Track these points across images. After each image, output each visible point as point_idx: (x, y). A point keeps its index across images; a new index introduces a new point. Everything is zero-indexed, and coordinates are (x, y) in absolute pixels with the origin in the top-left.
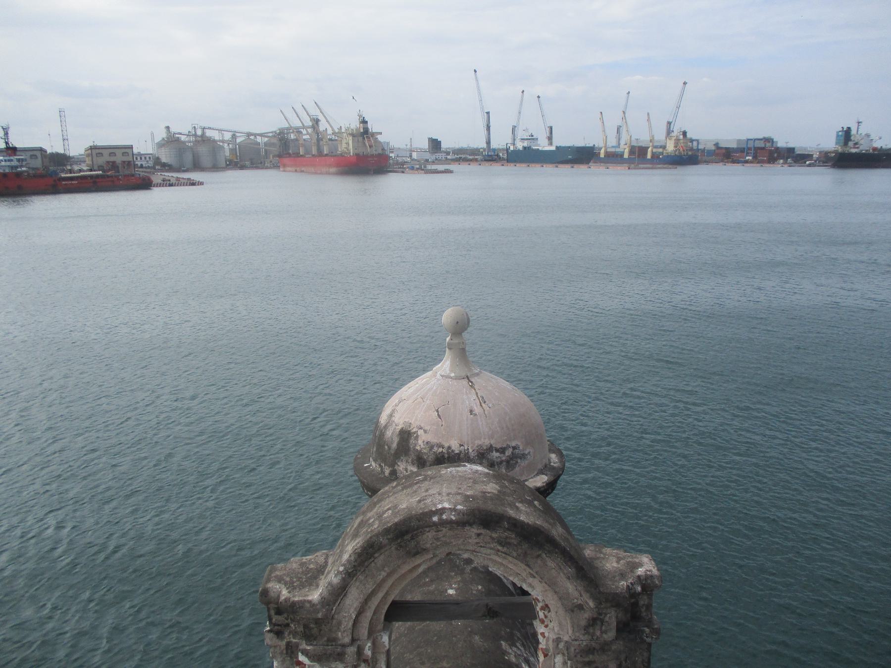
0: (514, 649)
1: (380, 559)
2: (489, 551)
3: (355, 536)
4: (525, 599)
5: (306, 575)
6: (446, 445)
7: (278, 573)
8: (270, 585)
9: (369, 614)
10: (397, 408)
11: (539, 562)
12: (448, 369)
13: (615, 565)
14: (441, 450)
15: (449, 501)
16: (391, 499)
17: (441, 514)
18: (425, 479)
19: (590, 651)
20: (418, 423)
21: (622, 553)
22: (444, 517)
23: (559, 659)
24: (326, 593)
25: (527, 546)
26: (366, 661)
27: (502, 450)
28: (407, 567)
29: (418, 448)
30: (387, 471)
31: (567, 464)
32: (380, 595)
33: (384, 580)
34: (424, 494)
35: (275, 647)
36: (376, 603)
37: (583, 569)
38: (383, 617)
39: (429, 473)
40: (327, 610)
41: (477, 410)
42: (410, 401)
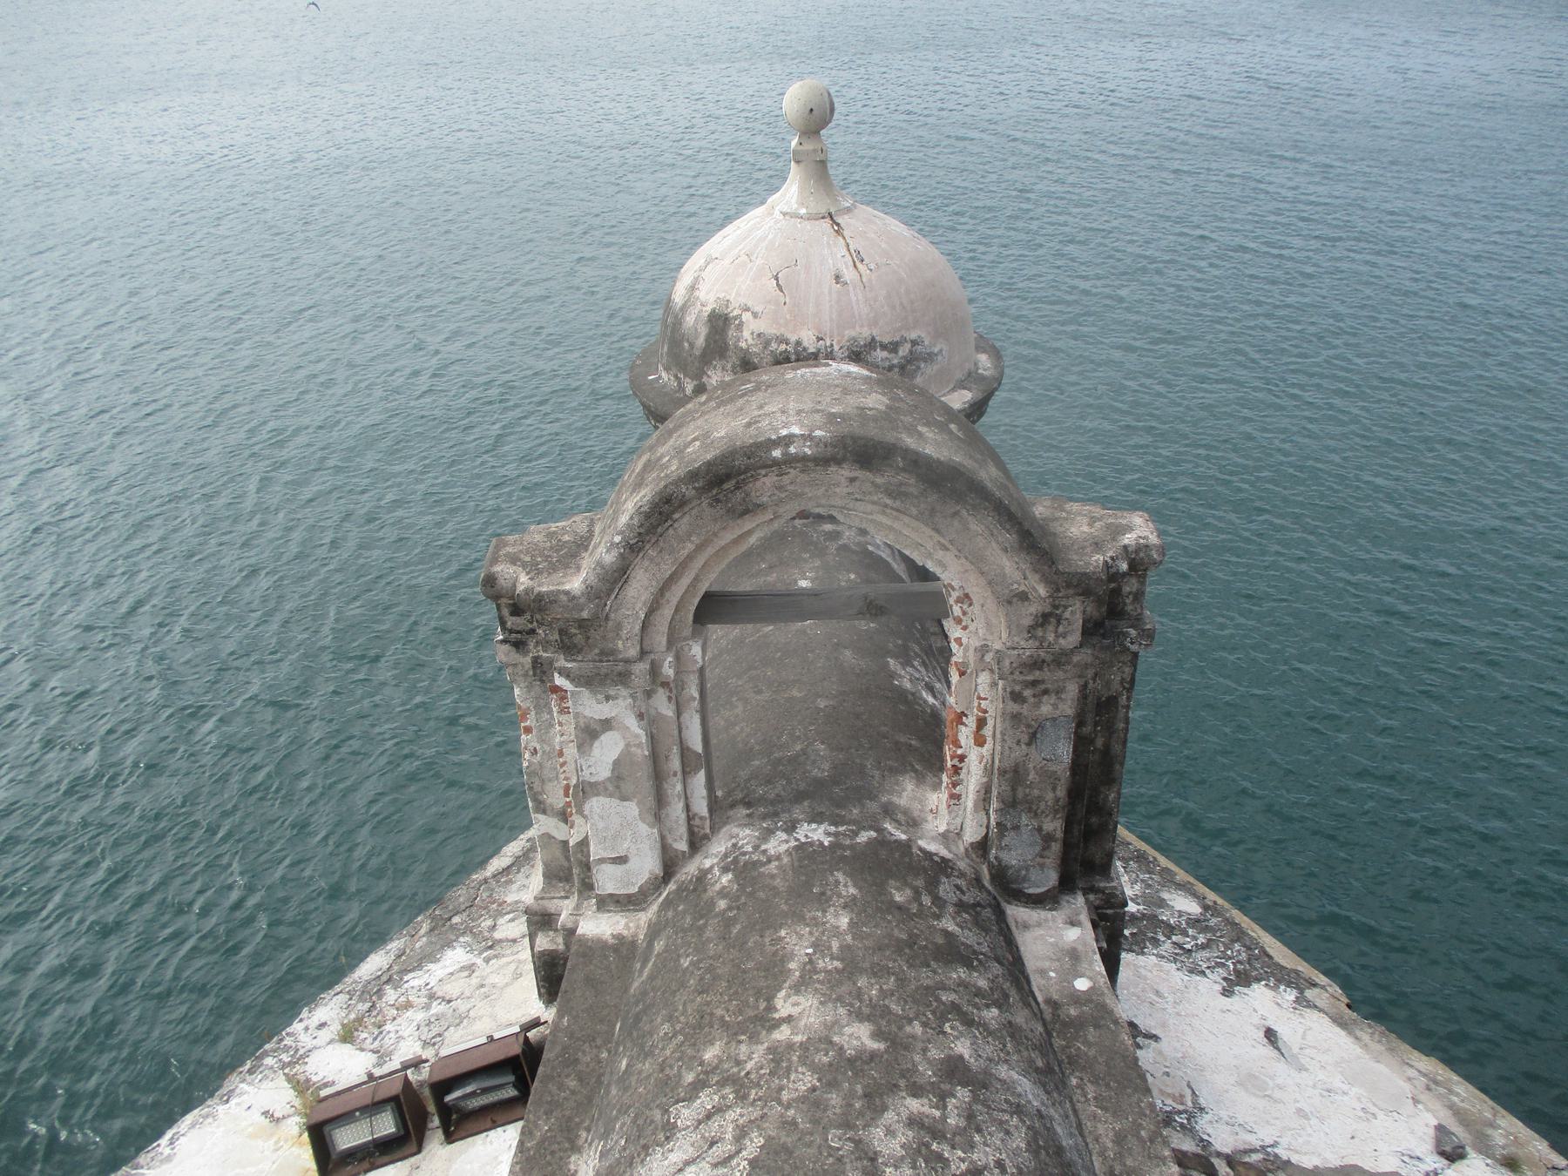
0: (909, 669)
1: (683, 523)
2: (869, 507)
3: (638, 485)
4: (929, 586)
5: (557, 551)
6: (793, 338)
7: (509, 549)
8: (497, 568)
9: (667, 612)
10: (703, 274)
11: (956, 523)
12: (794, 200)
13: (1085, 529)
14: (783, 347)
15: (800, 423)
16: (699, 422)
17: (787, 445)
18: (757, 389)
19: (1036, 664)
20: (742, 300)
21: (1098, 511)
22: (792, 450)
23: (984, 679)
24: (593, 580)
25: (935, 497)
26: (665, 685)
27: (893, 347)
28: (729, 537)
29: (743, 345)
30: (689, 387)
31: (1007, 371)
32: (685, 581)
33: (690, 557)
34: (756, 413)
35: (515, 665)
36: (680, 594)
37: (1031, 534)
38: (691, 617)
39: (765, 378)
40: (597, 606)
41: (849, 275)
42: (727, 261)
